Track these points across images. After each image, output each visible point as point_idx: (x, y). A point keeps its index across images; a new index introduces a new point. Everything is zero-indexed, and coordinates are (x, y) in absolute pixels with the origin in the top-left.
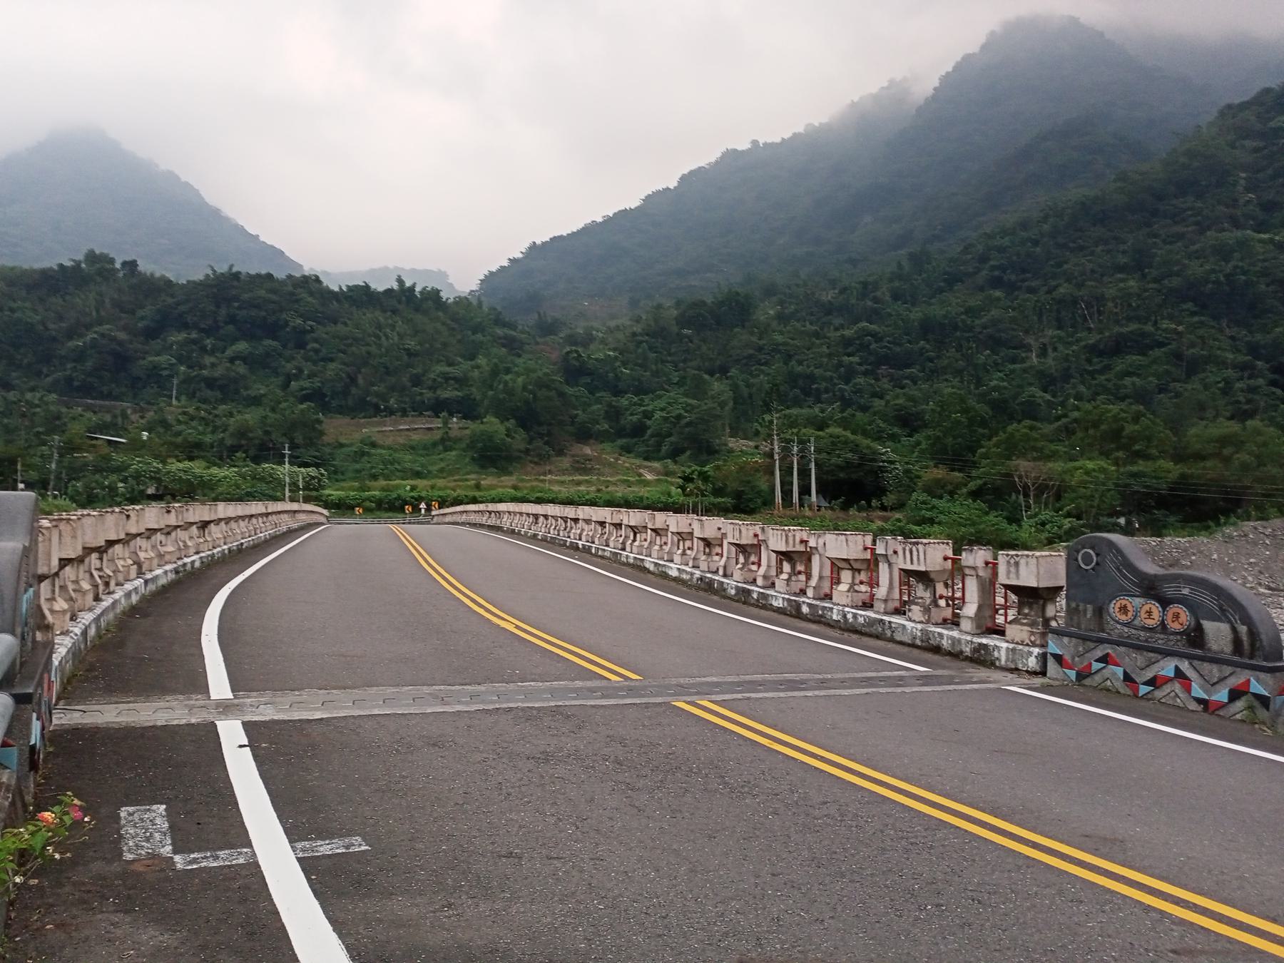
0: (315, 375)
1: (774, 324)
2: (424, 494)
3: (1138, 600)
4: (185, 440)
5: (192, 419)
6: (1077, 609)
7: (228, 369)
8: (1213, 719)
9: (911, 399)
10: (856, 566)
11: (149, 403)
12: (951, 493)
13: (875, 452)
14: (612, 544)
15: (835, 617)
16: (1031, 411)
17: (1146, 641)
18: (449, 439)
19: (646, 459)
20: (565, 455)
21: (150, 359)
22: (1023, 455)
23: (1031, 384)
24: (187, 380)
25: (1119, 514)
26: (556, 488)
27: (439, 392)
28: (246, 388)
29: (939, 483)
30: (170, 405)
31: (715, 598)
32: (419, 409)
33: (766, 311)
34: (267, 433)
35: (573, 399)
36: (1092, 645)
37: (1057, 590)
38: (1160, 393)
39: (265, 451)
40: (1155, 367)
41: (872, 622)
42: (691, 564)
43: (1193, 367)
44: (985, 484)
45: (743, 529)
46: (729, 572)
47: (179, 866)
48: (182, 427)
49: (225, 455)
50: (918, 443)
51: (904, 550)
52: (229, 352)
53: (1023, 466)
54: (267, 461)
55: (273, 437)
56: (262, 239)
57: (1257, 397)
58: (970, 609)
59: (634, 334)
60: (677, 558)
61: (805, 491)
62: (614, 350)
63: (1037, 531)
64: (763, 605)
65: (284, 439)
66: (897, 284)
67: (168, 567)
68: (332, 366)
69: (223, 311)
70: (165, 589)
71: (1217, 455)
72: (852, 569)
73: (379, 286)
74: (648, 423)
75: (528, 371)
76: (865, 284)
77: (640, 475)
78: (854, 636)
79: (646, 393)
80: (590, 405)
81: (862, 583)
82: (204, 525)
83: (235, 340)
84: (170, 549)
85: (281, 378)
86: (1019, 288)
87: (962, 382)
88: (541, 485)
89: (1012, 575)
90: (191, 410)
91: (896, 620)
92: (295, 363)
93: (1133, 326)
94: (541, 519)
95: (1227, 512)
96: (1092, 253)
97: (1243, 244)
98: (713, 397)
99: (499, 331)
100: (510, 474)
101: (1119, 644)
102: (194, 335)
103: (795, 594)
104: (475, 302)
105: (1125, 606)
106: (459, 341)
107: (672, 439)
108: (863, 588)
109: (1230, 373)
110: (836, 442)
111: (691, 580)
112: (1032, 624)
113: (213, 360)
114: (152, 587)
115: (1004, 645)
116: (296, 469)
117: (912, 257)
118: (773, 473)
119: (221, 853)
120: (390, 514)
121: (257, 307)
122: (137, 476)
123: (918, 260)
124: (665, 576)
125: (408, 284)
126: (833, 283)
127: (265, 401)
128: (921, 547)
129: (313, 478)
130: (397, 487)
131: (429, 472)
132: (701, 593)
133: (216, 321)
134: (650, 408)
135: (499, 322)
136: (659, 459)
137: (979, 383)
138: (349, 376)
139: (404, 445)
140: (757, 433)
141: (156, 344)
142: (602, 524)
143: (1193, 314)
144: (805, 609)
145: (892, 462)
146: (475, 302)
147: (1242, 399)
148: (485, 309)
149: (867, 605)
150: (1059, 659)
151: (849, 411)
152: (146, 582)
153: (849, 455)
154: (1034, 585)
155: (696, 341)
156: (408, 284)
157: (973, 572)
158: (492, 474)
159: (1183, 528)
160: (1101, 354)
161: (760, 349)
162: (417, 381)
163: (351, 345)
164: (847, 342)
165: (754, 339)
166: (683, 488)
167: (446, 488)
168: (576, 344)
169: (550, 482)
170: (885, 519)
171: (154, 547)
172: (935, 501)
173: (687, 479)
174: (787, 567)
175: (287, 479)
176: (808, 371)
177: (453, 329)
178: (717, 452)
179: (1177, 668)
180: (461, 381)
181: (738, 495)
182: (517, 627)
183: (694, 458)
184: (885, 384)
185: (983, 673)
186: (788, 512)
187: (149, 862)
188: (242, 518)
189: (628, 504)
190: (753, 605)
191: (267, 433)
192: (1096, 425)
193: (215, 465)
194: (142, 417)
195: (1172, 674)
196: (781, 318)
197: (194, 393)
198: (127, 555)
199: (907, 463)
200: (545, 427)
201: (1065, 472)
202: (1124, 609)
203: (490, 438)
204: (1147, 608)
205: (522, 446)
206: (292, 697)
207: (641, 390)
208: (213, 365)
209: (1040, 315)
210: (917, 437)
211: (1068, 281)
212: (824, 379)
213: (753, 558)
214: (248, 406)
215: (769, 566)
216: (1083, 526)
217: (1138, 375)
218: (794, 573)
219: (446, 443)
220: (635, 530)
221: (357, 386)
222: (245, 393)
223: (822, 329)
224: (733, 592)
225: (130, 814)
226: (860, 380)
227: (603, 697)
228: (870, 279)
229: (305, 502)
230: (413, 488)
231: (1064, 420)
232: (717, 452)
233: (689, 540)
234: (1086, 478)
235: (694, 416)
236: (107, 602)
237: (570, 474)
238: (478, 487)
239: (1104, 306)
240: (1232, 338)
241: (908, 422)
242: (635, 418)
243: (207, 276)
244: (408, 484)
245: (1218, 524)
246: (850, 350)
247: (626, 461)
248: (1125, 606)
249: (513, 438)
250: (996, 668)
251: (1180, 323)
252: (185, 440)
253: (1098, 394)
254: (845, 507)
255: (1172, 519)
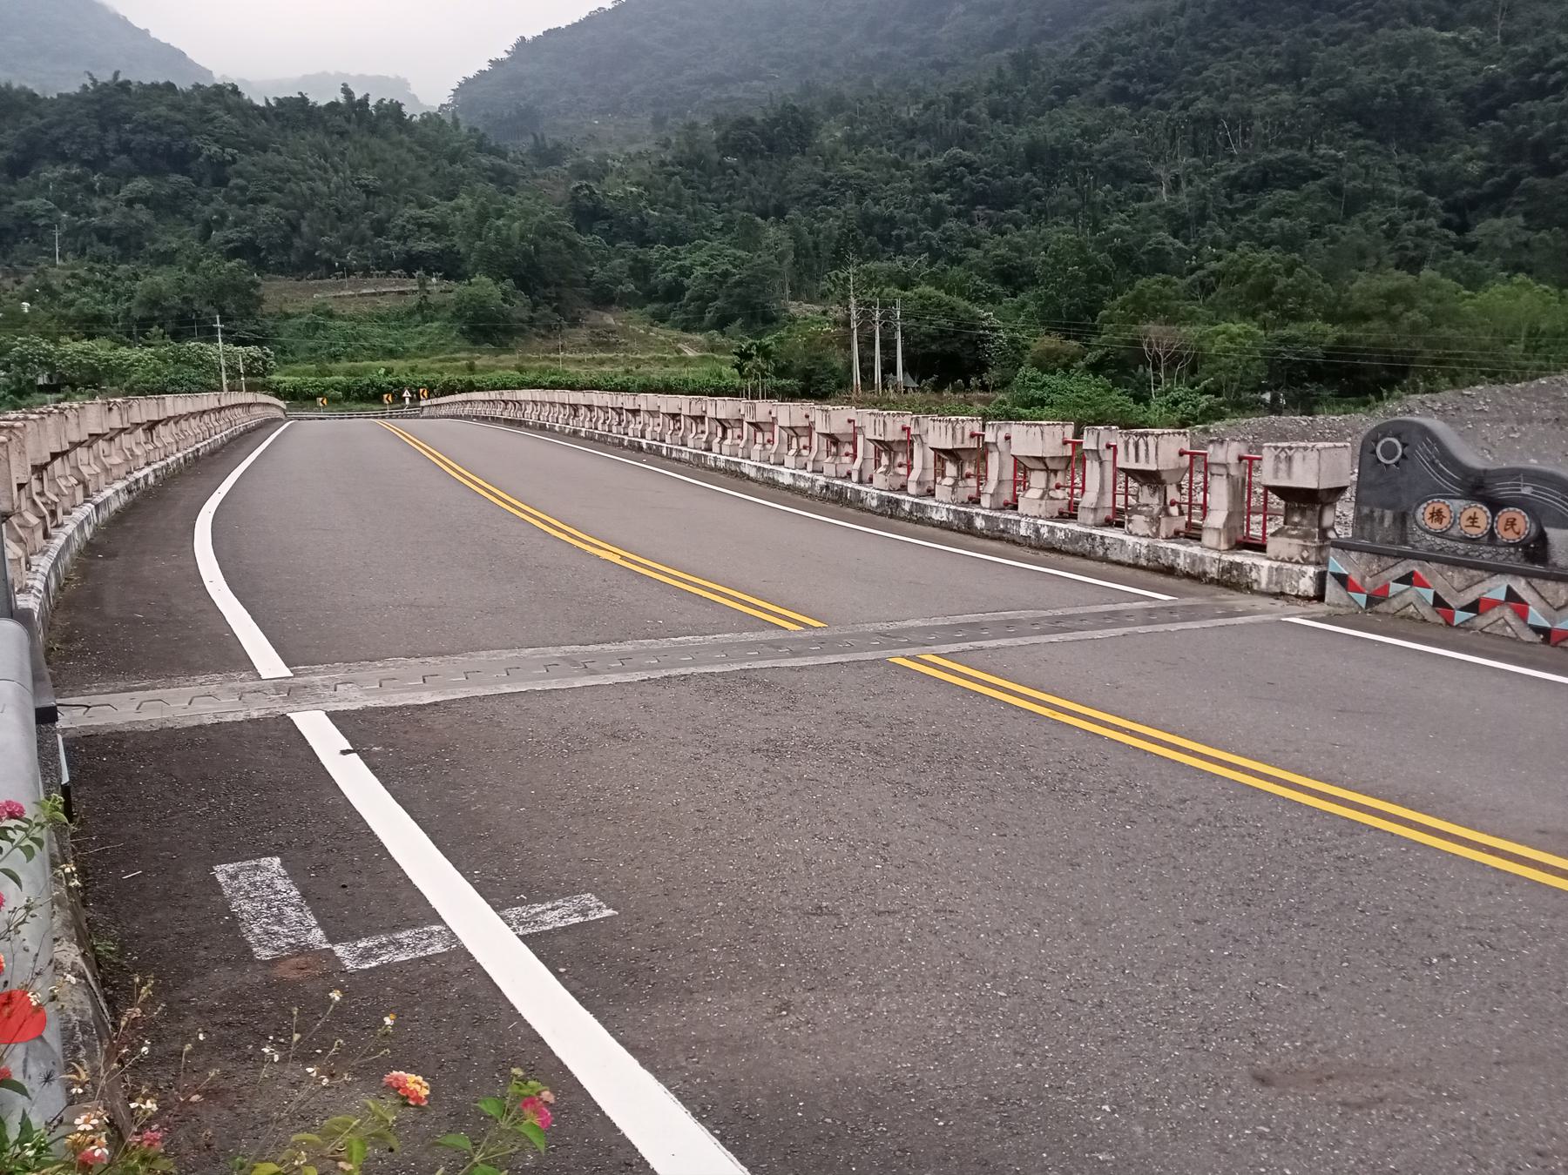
0: (244, 222)
1: (844, 149)
2: (403, 378)
3: (1457, 503)
4: (80, 311)
5: (85, 283)
6: (1370, 517)
7: (125, 216)
8: (1556, 651)
9: (1018, 249)
10: (1052, 466)
11: (24, 264)
12: (1066, 367)
13: (975, 317)
14: (690, 443)
15: (1023, 532)
16: (1159, 262)
17: (1466, 555)
18: (429, 306)
19: (685, 329)
20: (581, 326)
21: (20, 203)
22: (1154, 315)
23: (1159, 228)
24: (73, 232)
25: (1264, 389)
26: (572, 369)
27: (410, 243)
28: (154, 241)
29: (1052, 355)
30: (54, 265)
31: (850, 510)
32: (386, 265)
33: (832, 133)
34: (186, 300)
35: (587, 251)
36: (1391, 561)
37: (1339, 491)
38: (1312, 237)
39: (185, 325)
40: (1308, 204)
41: (1079, 537)
42: (810, 468)
43: (1353, 205)
44: (1107, 354)
45: (889, 421)
46: (866, 477)
47: (350, 965)
48: (72, 295)
49: (137, 330)
50: (1024, 305)
51: (1127, 443)
52: (125, 192)
53: (1154, 332)
54: (190, 337)
55: (196, 306)
56: (153, 34)
57: (1427, 242)
58: (1217, 518)
59: (663, 164)
60: (790, 460)
61: (889, 368)
62: (638, 184)
63: (1170, 411)
64: (917, 517)
65: (209, 309)
66: (995, 96)
67: (119, 485)
68: (265, 209)
69: (112, 136)
70: (121, 516)
71: (1383, 314)
72: (1047, 470)
73: (320, 99)
74: (687, 282)
75: (527, 213)
76: (957, 98)
77: (679, 351)
78: (1053, 556)
79: (682, 243)
80: (609, 259)
81: (1058, 487)
82: (151, 426)
83: (131, 176)
84: (117, 460)
85: (198, 227)
86: (1147, 103)
87: (1076, 225)
88: (553, 365)
89: (1282, 474)
90: (82, 272)
91: (1111, 534)
92: (213, 205)
93: (1284, 152)
94: (583, 411)
95: (1390, 384)
96: (1239, 56)
97: (1421, 46)
98: (768, 247)
99: (485, 161)
100: (511, 351)
101: (1428, 559)
102: (75, 170)
103: (963, 504)
104: (449, 120)
105: (1439, 511)
106: (432, 174)
107: (718, 303)
108: (1060, 494)
109: (1396, 211)
110: (926, 305)
111: (812, 488)
112: (1306, 536)
113: (103, 203)
114: (104, 513)
115: (1267, 563)
116: (230, 347)
117: (1015, 59)
118: (849, 347)
119: (404, 936)
120: (364, 406)
121: (158, 129)
122: (23, 361)
123: (1024, 65)
124: (774, 484)
125: (358, 96)
126: (916, 95)
127: (179, 257)
128: (1151, 439)
129: (256, 360)
130: (366, 370)
131: (407, 350)
132: (829, 506)
133: (103, 150)
134: (687, 263)
135: (481, 147)
136: (702, 330)
137: (1096, 228)
138: (288, 221)
139: (371, 315)
140: (824, 296)
141: (25, 182)
142: (675, 417)
143: (1357, 136)
144: (979, 523)
145: (994, 330)
146: (449, 120)
147: (1409, 243)
148: (464, 129)
149: (1070, 514)
150: (1342, 580)
151: (941, 263)
152: (97, 507)
153: (943, 321)
154: (1313, 485)
155: (743, 172)
156: (358, 96)
157: (1222, 471)
158: (488, 351)
159: (1338, 404)
160: (1244, 188)
161: (826, 184)
162: (380, 228)
163: (289, 180)
164: (934, 175)
165: (818, 170)
166: (739, 367)
167: (429, 371)
168: (585, 176)
169: (564, 361)
170: (987, 402)
171: (97, 458)
172: (1047, 378)
173: (745, 356)
174: (951, 469)
175: (223, 362)
176: (887, 213)
177: (423, 158)
178: (775, 320)
179: (1509, 589)
180: (440, 229)
181: (807, 375)
182: (622, 557)
183: (746, 327)
184: (982, 229)
185: (1240, 601)
186: (868, 396)
187: (301, 960)
188: (192, 414)
189: (668, 389)
190: (904, 519)
191: (186, 300)
192: (1241, 278)
193: (123, 344)
194: (18, 283)
195: (1502, 597)
196: (853, 142)
197: (83, 250)
198: (68, 472)
199: (1013, 330)
200: (553, 289)
201: (1202, 338)
202: (1437, 515)
203: (483, 305)
204: (1470, 513)
205: (525, 314)
206: (378, 670)
207: (674, 239)
208: (106, 211)
209: (1173, 138)
210: (1022, 296)
211: (1207, 92)
212: (907, 224)
213: (900, 459)
214: (158, 265)
215: (924, 469)
216: (1223, 404)
217: (1288, 215)
218: (962, 476)
219: (425, 311)
220: (724, 424)
221: (301, 236)
222: (152, 248)
223: (903, 156)
224: (874, 503)
225: (234, 877)
226: (951, 224)
227: (794, 654)
228: (964, 90)
229: (248, 390)
230: (388, 372)
231: (1200, 273)
232: (775, 320)
233: (788, 436)
234: (1228, 344)
235: (745, 273)
236: (59, 542)
237: (589, 351)
238: (471, 368)
239: (1251, 125)
240: (1402, 167)
241: (1012, 277)
242: (668, 276)
243: (85, 87)
244: (381, 365)
245: (1380, 398)
246: (938, 185)
247: (660, 333)
248: (1439, 511)
249: (512, 304)
250: (1254, 592)
251: (1341, 149)
252: (80, 311)
253: (1240, 240)
254: (938, 388)
255: (1326, 393)
